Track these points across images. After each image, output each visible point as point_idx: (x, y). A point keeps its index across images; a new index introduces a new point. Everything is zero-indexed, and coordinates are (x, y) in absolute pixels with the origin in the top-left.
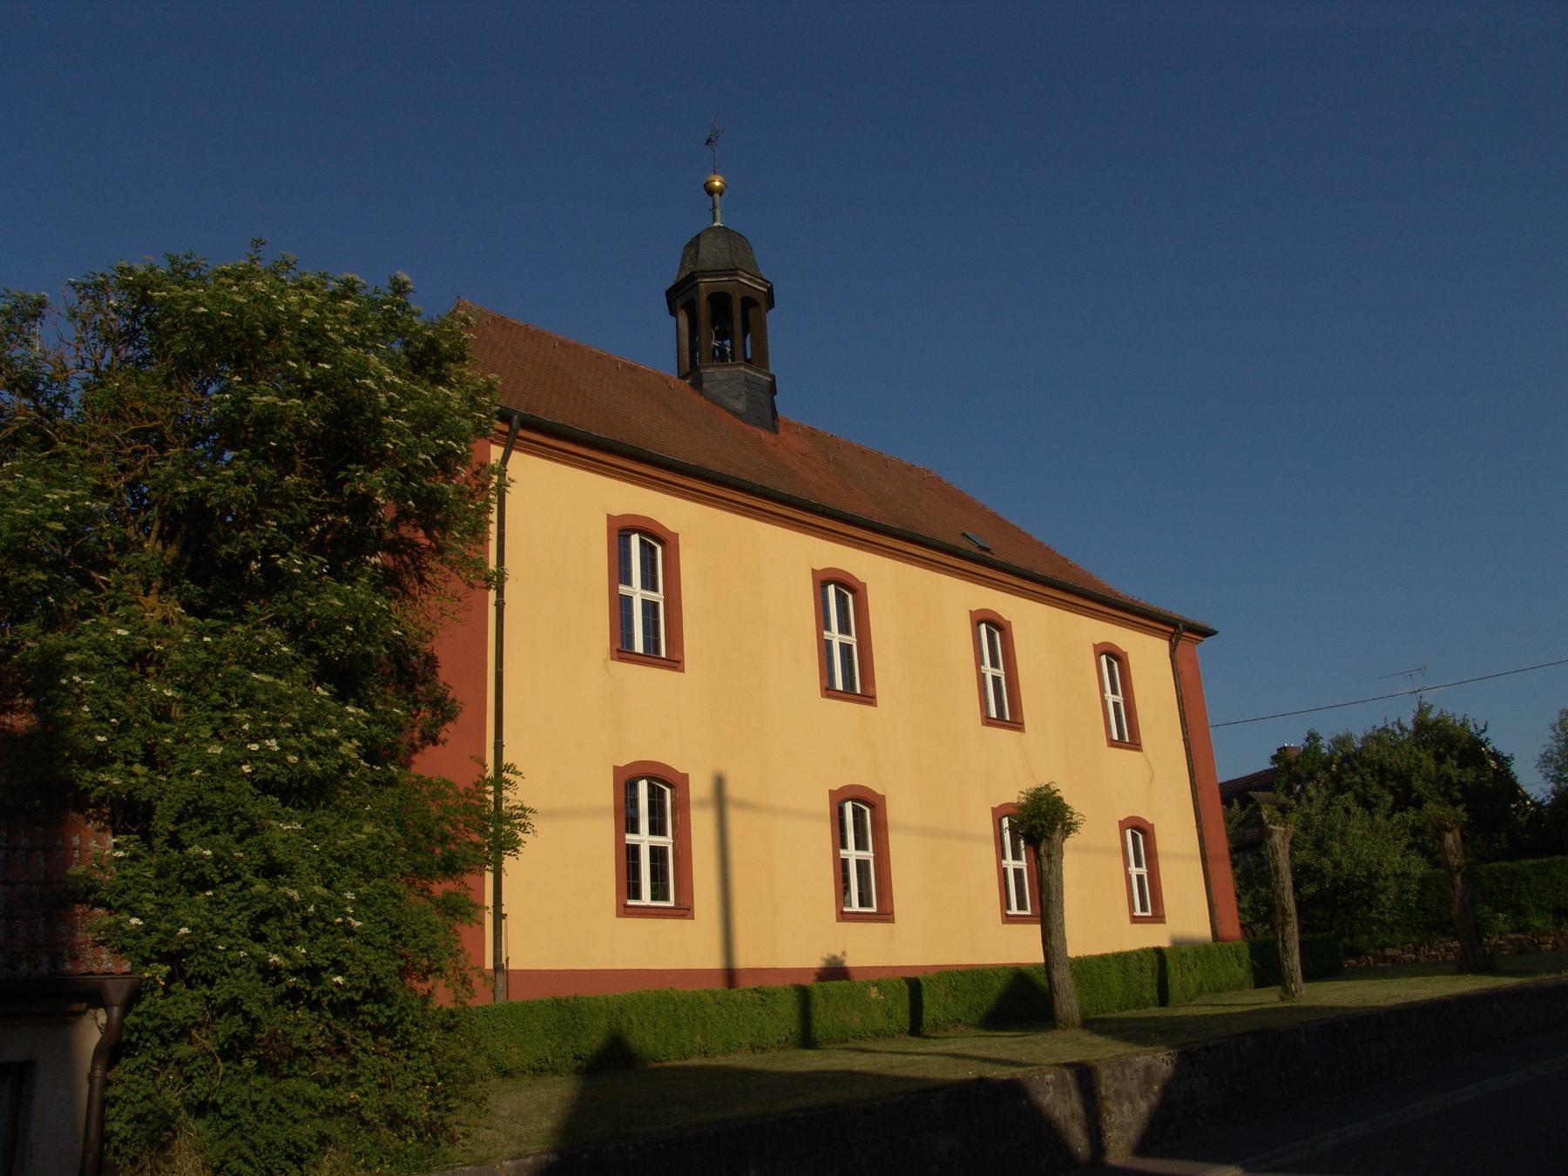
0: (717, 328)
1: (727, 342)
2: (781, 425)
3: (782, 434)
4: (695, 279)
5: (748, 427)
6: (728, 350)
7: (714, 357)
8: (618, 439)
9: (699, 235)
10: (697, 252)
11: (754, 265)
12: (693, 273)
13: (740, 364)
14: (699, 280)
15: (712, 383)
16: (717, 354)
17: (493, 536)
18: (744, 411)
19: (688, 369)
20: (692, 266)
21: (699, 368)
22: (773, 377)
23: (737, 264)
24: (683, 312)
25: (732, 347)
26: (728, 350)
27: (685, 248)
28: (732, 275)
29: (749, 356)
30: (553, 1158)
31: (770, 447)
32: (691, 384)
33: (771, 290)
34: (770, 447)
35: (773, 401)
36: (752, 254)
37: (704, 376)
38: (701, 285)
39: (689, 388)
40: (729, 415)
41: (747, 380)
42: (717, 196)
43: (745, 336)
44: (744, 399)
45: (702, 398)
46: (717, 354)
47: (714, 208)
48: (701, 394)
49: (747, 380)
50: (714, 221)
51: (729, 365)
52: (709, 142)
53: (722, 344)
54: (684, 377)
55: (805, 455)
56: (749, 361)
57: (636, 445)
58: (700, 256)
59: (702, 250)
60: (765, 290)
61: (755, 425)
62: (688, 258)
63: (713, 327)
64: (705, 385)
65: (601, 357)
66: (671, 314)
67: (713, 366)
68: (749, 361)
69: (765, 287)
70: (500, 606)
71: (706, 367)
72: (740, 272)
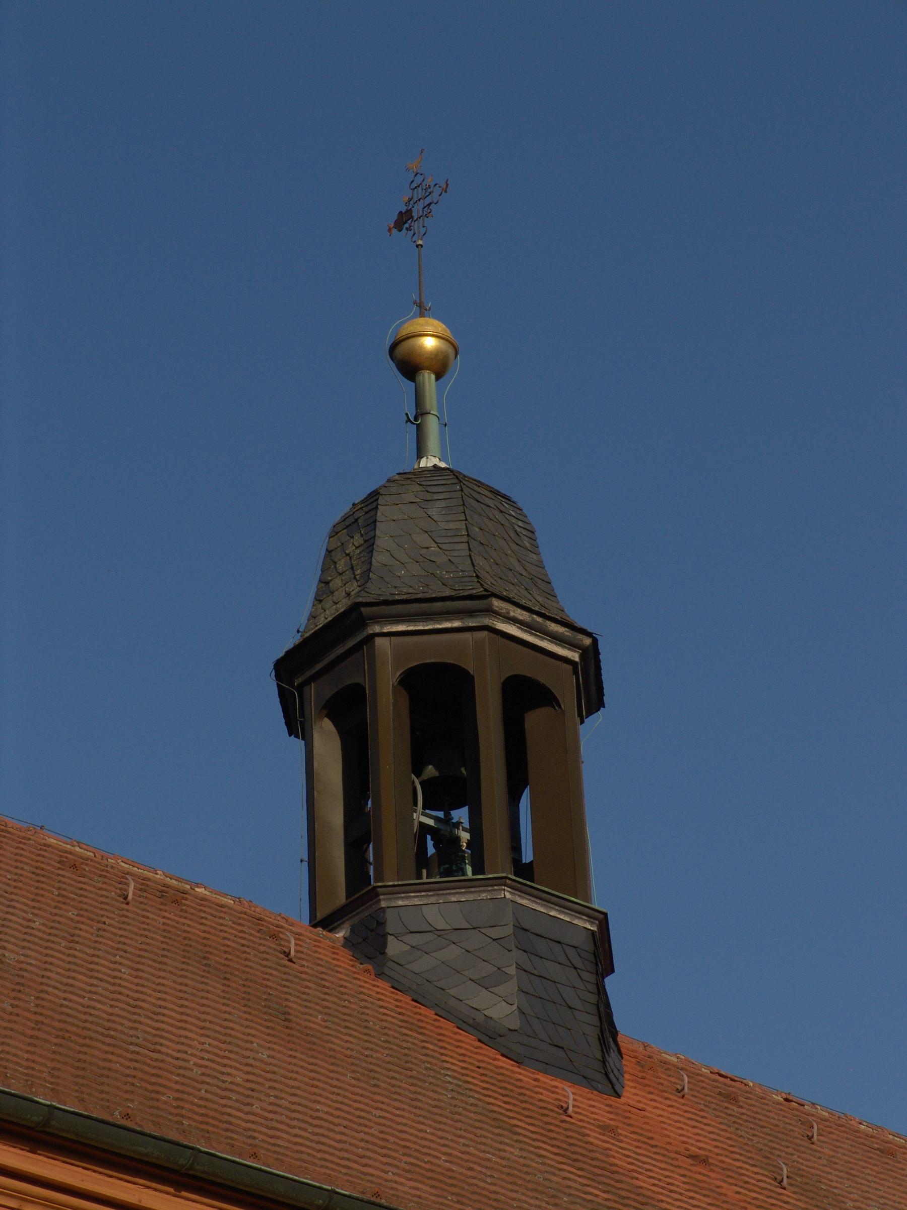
0: (430, 771)
1: (461, 815)
2: (628, 1065)
3: (631, 1093)
4: (363, 622)
5: (525, 1075)
6: (465, 836)
7: (422, 860)
8: (117, 1117)
9: (375, 495)
10: (369, 545)
11: (544, 583)
12: (356, 607)
13: (501, 881)
14: (377, 629)
15: (415, 939)
16: (431, 850)
17: (525, 882)
18: (515, 1023)
19: (341, 898)
20: (354, 587)
21: (374, 894)
22: (603, 921)
23: (488, 580)
24: (327, 724)
25: (476, 829)
26: (465, 836)
27: (334, 533)
28: (471, 613)
29: (528, 856)
30: (433, 356)
31: (595, 1137)
32: (348, 943)
33: (592, 655)
34: (595, 1137)
35: (601, 991)
36: (535, 548)
37: (390, 916)
38: (379, 641)
39: (345, 957)
40: (469, 1040)
41: (521, 929)
42: (428, 378)
43: (514, 797)
44: (510, 988)
45: (384, 985)
46: (431, 850)
47: (421, 413)
48: (379, 975)
49: (521, 929)
50: (420, 456)
51: (469, 884)
52: (403, 220)
53: (447, 820)
54: (328, 923)
55: (704, 1161)
56: (524, 871)
57: (174, 1136)
58: (379, 558)
59: (383, 541)
60: (575, 656)
61: (546, 1066)
62: (341, 566)
63: (418, 772)
64: (394, 947)
65: (74, 865)
66: (292, 731)
67: (419, 888)
68: (524, 871)
69: (572, 645)
70: (168, 1193)
71: (396, 891)
72: (496, 603)
